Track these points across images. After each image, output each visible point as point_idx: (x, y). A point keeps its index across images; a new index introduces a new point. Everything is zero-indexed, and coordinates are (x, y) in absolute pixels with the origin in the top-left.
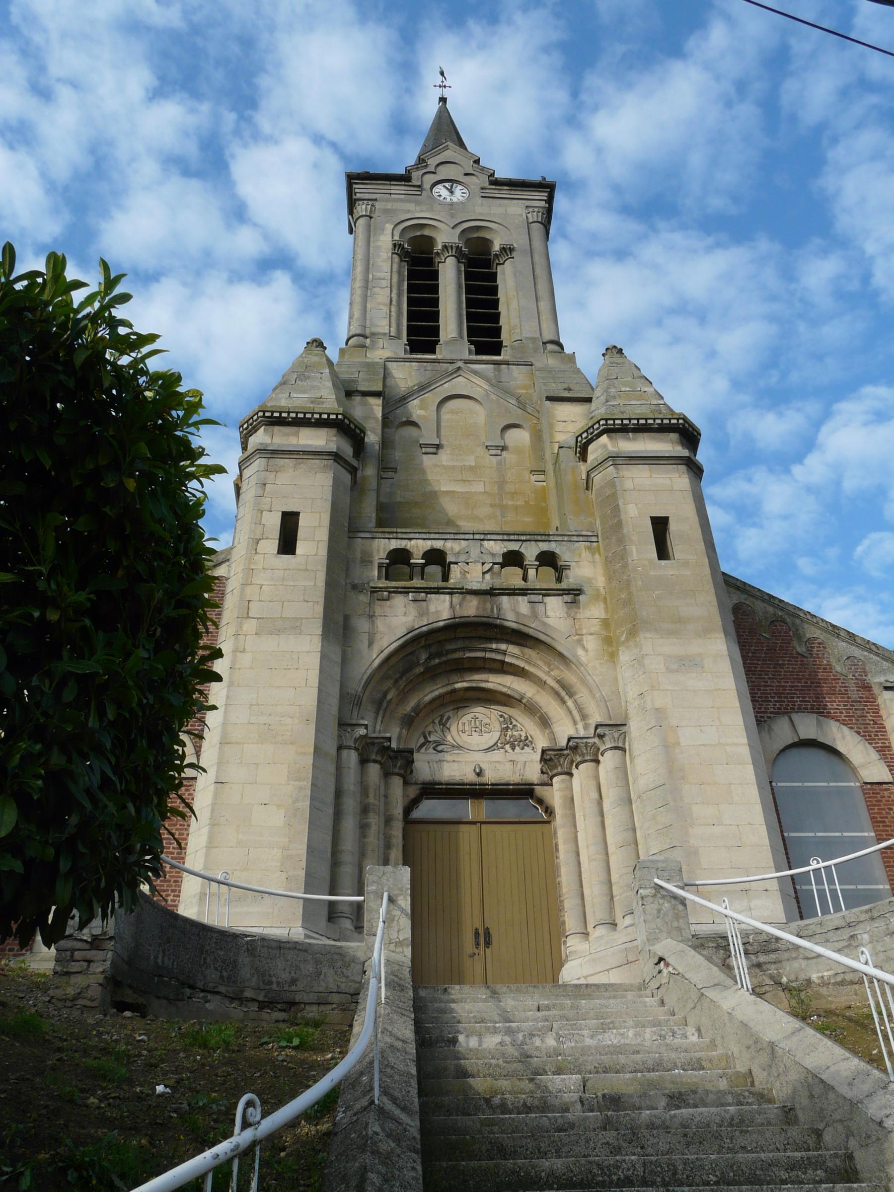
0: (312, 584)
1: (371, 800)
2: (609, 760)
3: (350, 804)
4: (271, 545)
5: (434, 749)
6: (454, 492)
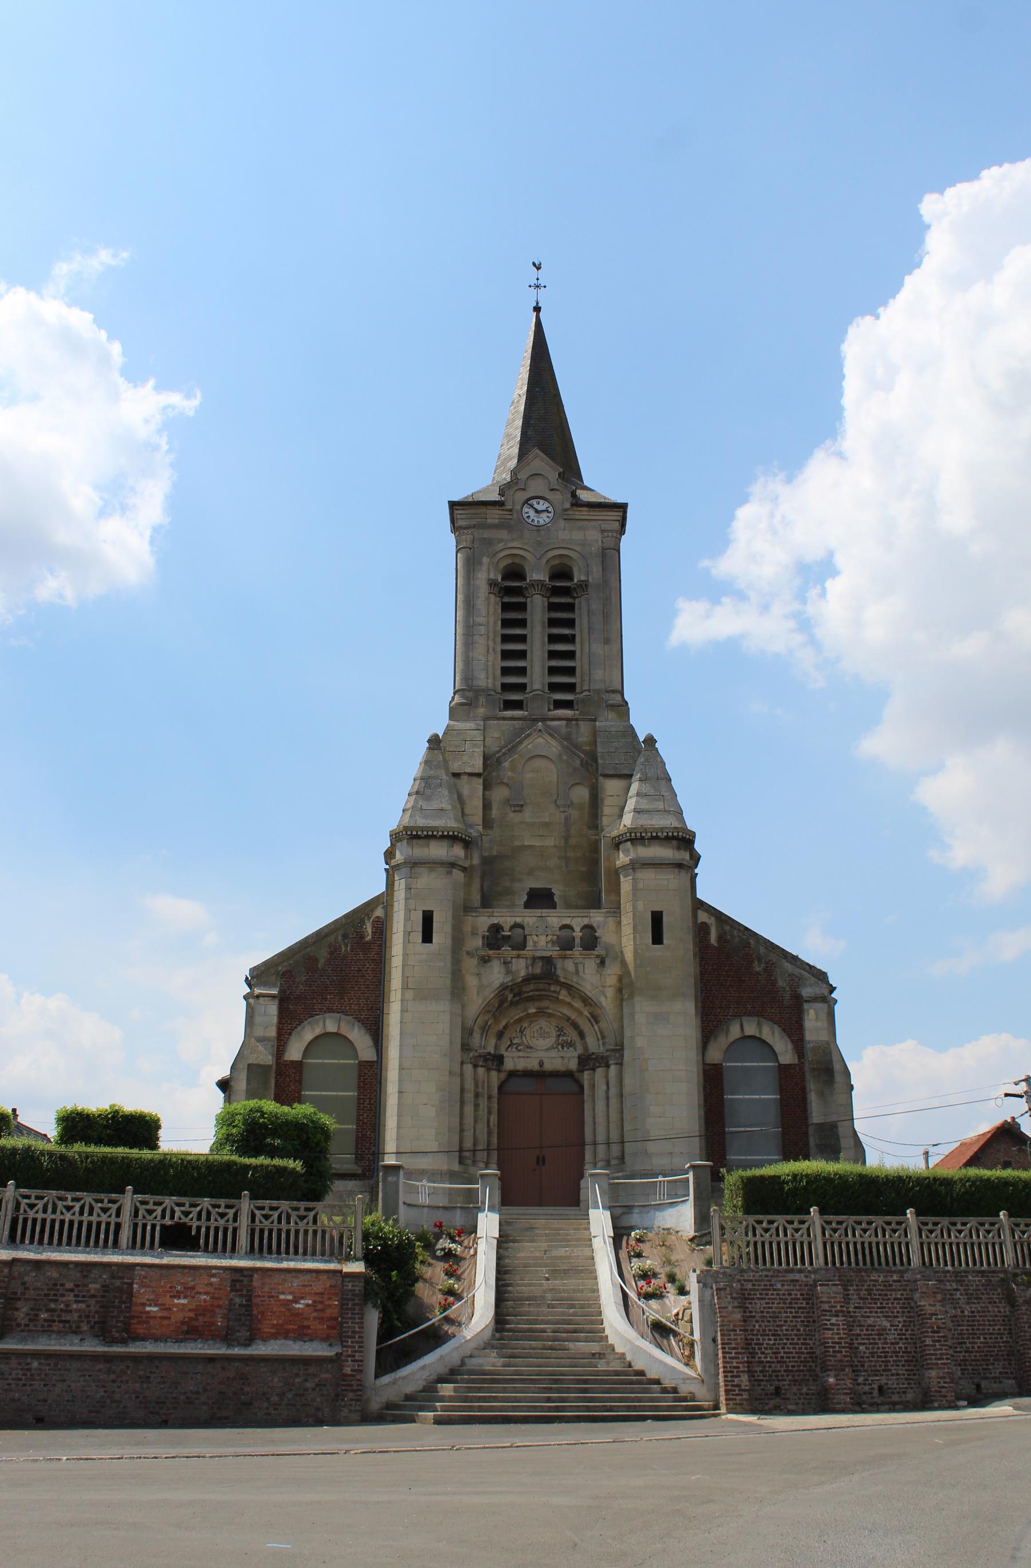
0: (443, 964)
1: (480, 1090)
2: (613, 1070)
3: (470, 1096)
4: (418, 936)
5: (516, 1048)
6: (533, 846)
